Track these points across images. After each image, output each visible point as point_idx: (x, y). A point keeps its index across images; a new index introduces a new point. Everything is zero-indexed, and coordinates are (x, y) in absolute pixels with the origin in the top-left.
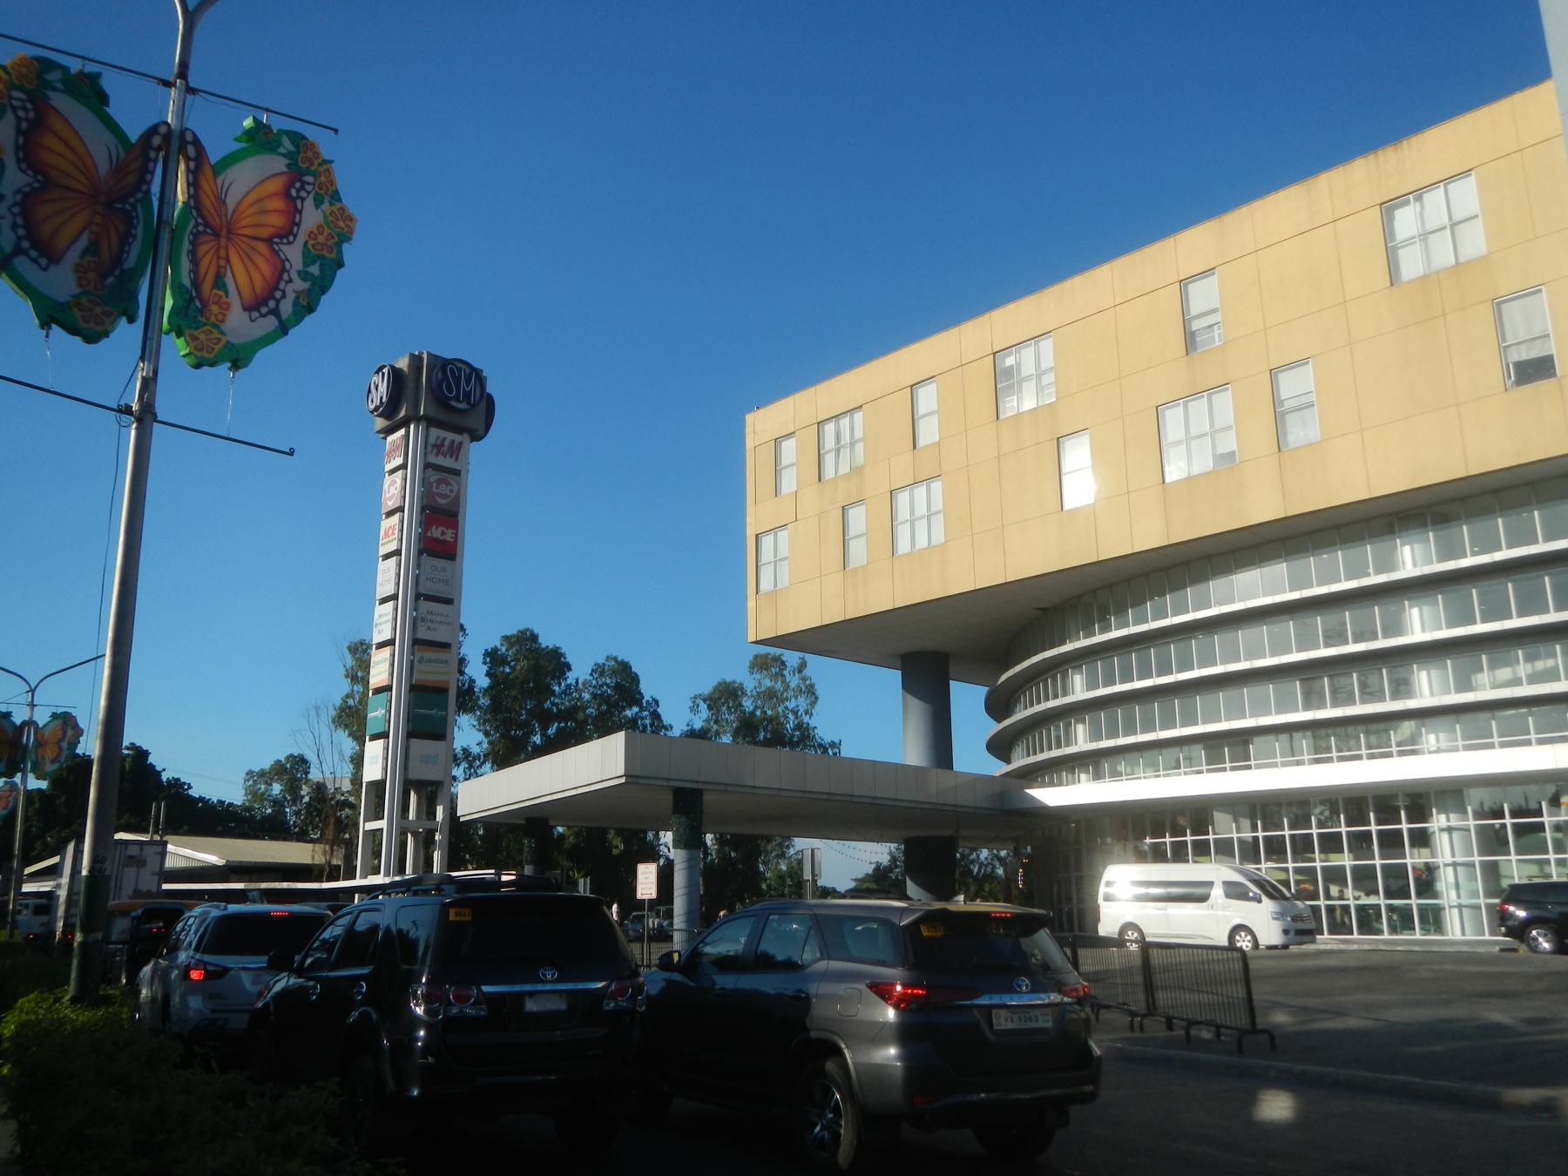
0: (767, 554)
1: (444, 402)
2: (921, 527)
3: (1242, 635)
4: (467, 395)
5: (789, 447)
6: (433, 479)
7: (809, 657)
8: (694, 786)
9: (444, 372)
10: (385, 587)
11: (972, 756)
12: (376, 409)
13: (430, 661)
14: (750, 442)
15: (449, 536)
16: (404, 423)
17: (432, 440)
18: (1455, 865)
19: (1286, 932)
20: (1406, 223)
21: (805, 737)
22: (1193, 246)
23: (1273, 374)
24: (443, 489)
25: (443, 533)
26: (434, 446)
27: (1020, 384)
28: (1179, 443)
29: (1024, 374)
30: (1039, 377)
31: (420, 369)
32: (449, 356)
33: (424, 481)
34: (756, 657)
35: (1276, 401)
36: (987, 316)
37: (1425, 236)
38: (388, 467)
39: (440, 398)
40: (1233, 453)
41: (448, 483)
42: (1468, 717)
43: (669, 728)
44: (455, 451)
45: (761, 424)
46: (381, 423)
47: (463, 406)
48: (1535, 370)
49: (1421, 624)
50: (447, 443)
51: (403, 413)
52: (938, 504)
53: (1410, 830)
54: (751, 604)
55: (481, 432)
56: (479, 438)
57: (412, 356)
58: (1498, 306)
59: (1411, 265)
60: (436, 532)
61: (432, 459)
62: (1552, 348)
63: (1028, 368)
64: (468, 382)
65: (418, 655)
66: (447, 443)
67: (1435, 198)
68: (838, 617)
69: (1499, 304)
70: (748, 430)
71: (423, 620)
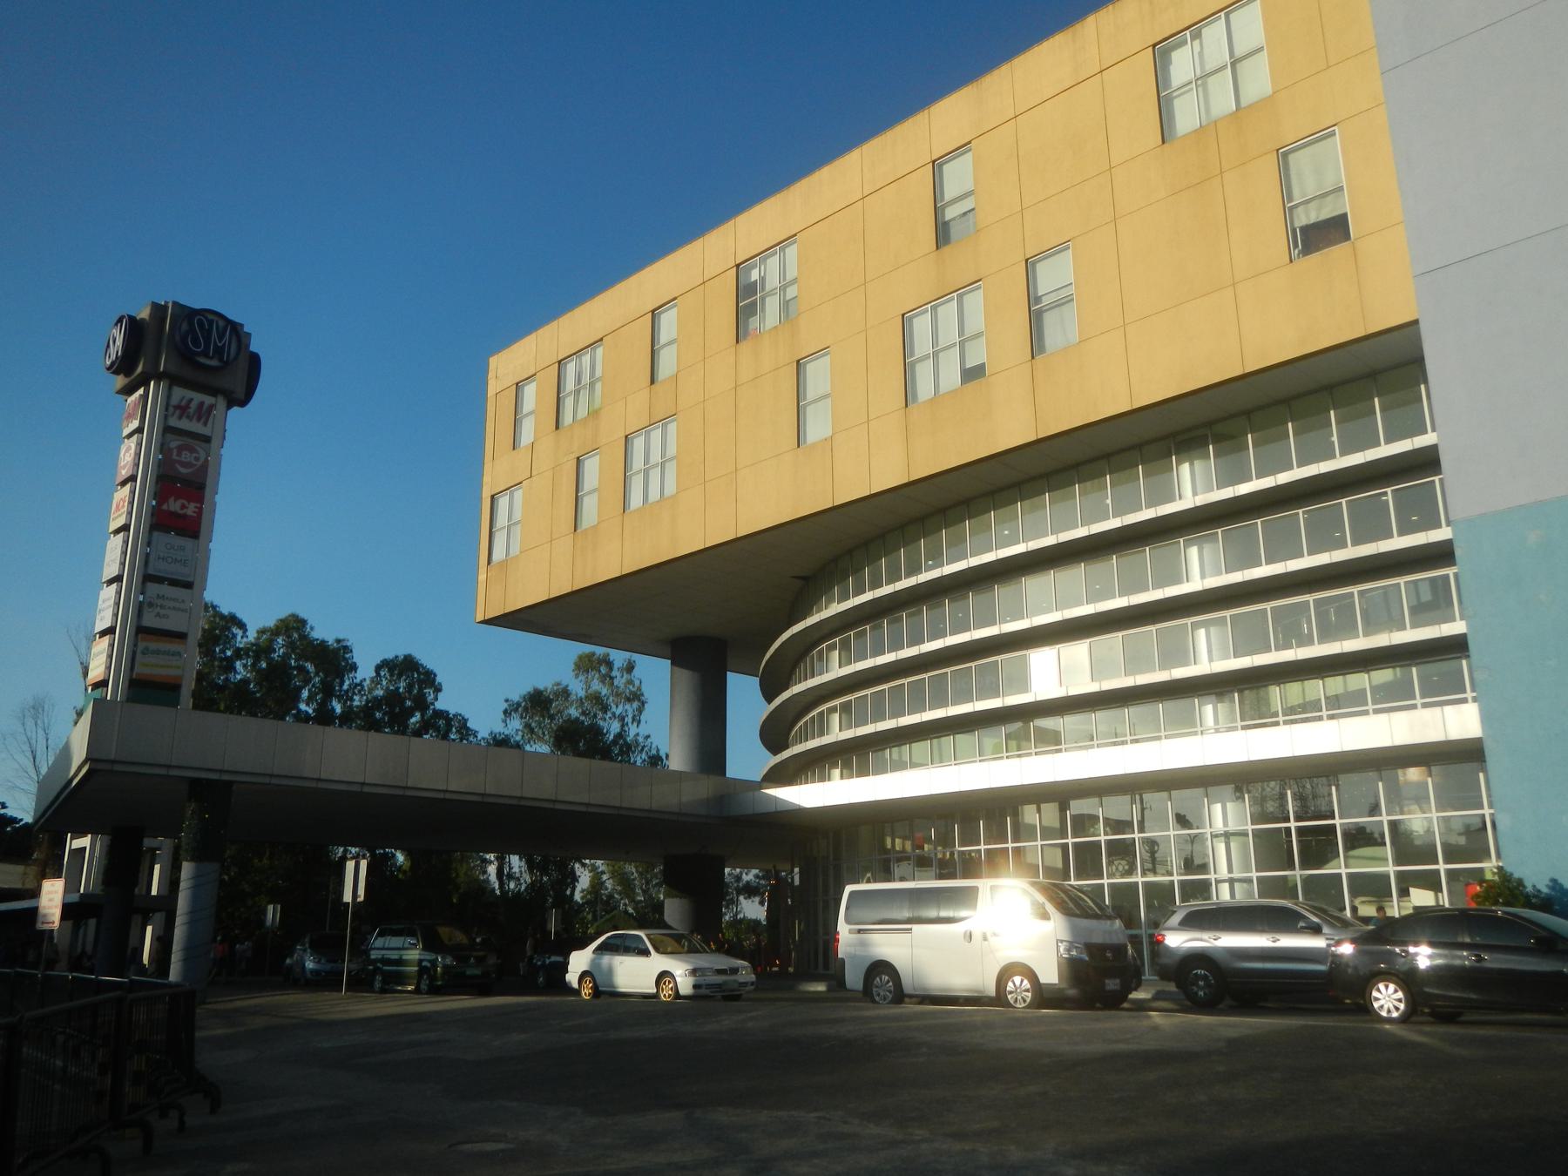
0: (502, 520)
1: (193, 362)
2: (655, 475)
3: (1001, 593)
4: (219, 352)
5: (530, 391)
6: (173, 445)
7: (635, 657)
8: (226, 777)
9: (191, 324)
10: (111, 570)
11: (746, 758)
12: (113, 364)
13: (157, 652)
14: (492, 389)
15: (191, 509)
16: (143, 382)
17: (175, 401)
18: (1231, 881)
19: (695, 987)
20: (1182, 65)
21: (625, 747)
22: (948, 118)
23: (1030, 265)
24: (186, 456)
25: (183, 507)
26: (177, 407)
27: (763, 299)
28: (927, 357)
29: (768, 288)
30: (783, 288)
31: (164, 319)
32: (197, 306)
33: (163, 448)
34: (580, 658)
35: (1032, 298)
36: (731, 223)
37: (1202, 79)
38: (126, 432)
39: (186, 356)
40: (983, 365)
41: (192, 450)
42: (1245, 688)
43: (475, 734)
44: (204, 414)
45: (505, 367)
46: (120, 381)
47: (214, 363)
48: (1332, 231)
49: (1200, 568)
50: (193, 405)
51: (140, 369)
52: (672, 450)
53: (1437, 863)
54: (482, 577)
55: (240, 394)
56: (243, 403)
57: (155, 306)
58: (1283, 158)
59: (1186, 117)
60: (174, 505)
61: (173, 422)
62: (1345, 205)
63: (773, 282)
64: (221, 337)
65: (141, 645)
66: (193, 405)
67: (1215, 33)
68: (566, 589)
69: (1285, 155)
70: (491, 375)
71: (151, 605)
